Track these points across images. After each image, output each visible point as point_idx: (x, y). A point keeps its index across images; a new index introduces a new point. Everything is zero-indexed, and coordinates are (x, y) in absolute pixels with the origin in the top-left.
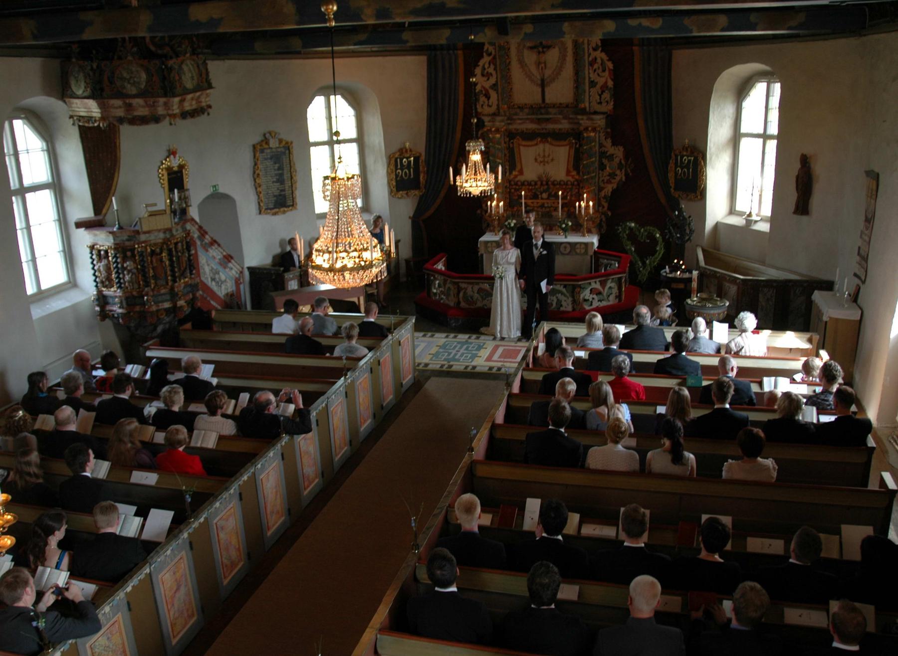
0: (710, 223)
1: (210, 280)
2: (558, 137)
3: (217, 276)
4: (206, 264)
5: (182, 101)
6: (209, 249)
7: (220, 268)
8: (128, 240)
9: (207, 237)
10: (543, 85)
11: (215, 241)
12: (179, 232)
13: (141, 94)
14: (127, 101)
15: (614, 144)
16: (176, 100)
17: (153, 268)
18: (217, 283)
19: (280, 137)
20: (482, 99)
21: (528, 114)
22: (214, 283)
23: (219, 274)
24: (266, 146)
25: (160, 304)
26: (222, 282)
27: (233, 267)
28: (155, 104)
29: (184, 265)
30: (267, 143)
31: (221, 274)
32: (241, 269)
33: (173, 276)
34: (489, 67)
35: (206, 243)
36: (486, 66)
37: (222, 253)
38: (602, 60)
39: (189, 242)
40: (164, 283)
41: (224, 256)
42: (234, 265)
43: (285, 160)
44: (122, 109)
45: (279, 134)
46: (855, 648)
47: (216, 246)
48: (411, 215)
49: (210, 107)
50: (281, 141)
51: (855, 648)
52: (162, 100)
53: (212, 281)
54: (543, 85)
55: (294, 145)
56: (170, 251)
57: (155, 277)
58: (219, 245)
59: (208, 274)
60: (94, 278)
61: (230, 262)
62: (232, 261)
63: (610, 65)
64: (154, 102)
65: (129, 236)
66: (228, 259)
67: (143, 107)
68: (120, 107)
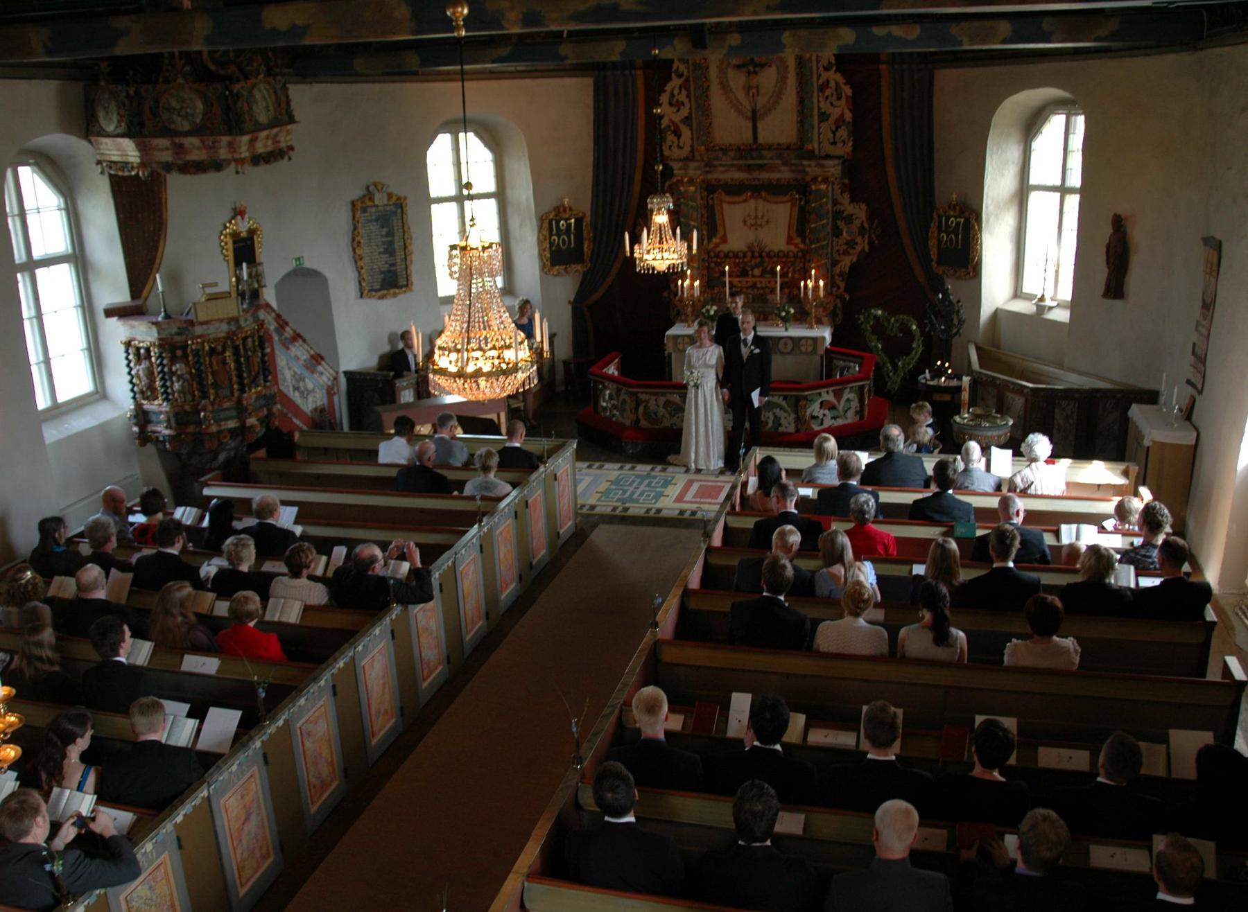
0: (986, 310)
1: (291, 389)
2: (776, 190)
3: (301, 384)
4: (286, 367)
5: (253, 141)
6: (291, 347)
7: (306, 373)
8: (178, 334)
9: (288, 329)
10: (754, 118)
11: (299, 336)
12: (248, 323)
13: (197, 131)
14: (177, 141)
15: (853, 200)
16: (245, 139)
17: (213, 373)
18: (302, 393)
19: (390, 190)
20: (670, 137)
21: (734, 159)
22: (297, 394)
23: (304, 381)
24: (370, 203)
25: (223, 423)
26: (309, 392)
27: (324, 371)
28: (216, 144)
29: (256, 369)
30: (371, 199)
31: (307, 380)
32: (334, 374)
33: (241, 383)
34: (680, 93)
35: (286, 338)
36: (676, 92)
37: (308, 352)
38: (837, 83)
39: (262, 337)
40: (228, 394)
41: (312, 356)
42: (325, 369)
43: (396, 222)
44: (170, 152)
45: (388, 186)
46: (1189, 901)
47: (300, 341)
48: (572, 300)
49: (291, 148)
50: (390, 196)
51: (1189, 901)
52: (225, 139)
53: (294, 391)
54: (754, 118)
55: (408, 201)
56: (236, 349)
57: (216, 385)
58: (304, 341)
59: (289, 381)
60: (130, 386)
61: (319, 364)
62: (323, 363)
63: (848, 90)
64: (214, 142)
65: (179, 328)
66: (316, 360)
67: (199, 148)
68: (167, 149)
